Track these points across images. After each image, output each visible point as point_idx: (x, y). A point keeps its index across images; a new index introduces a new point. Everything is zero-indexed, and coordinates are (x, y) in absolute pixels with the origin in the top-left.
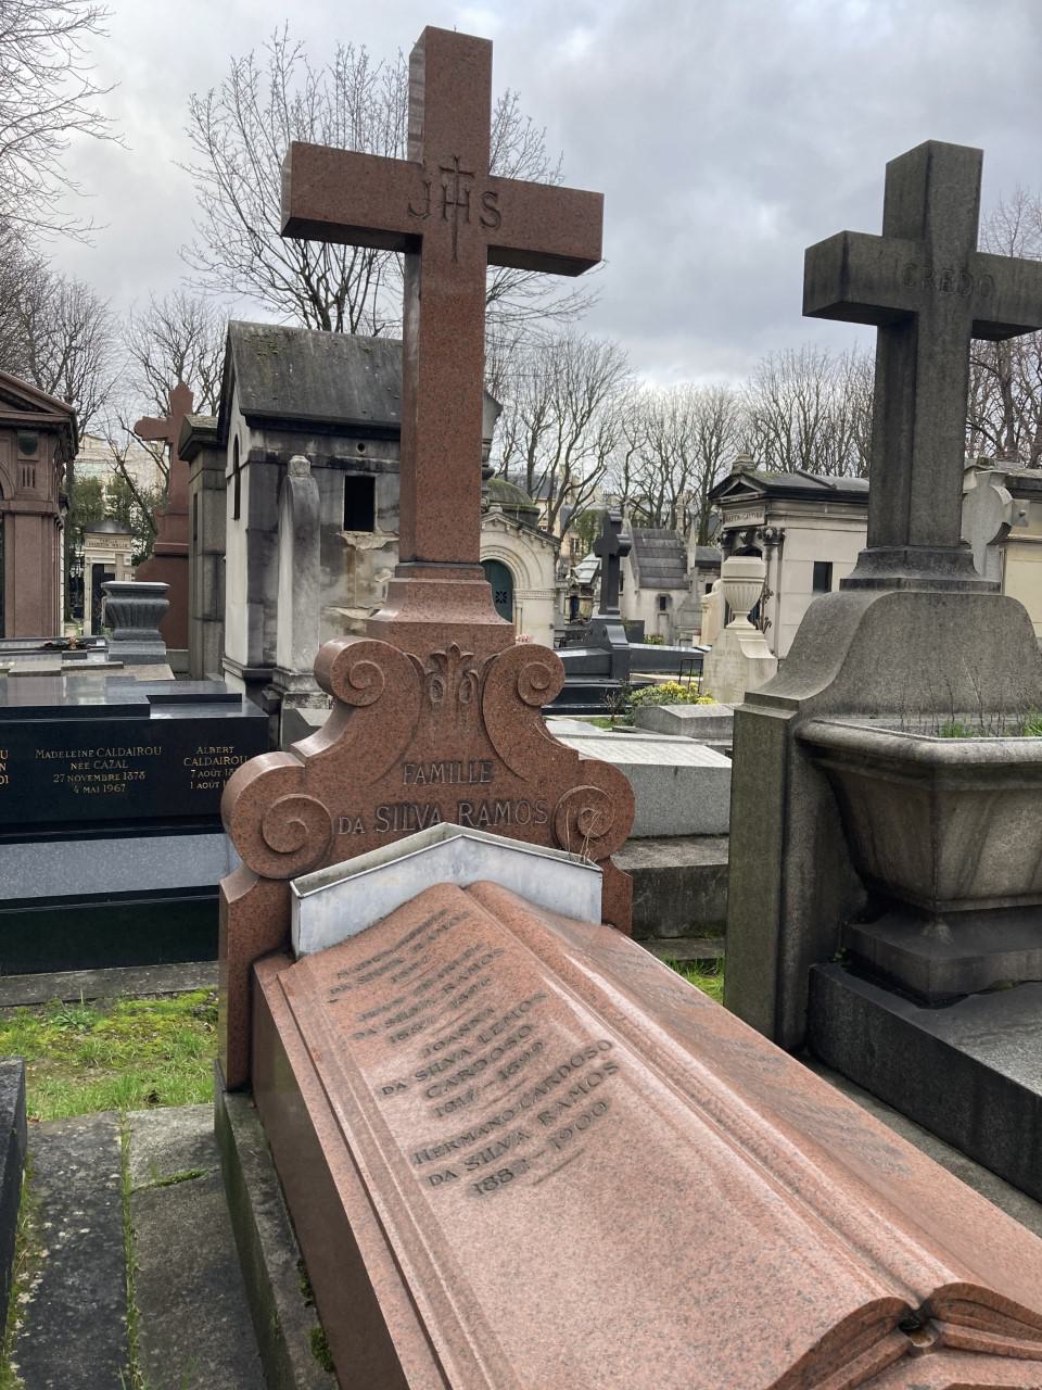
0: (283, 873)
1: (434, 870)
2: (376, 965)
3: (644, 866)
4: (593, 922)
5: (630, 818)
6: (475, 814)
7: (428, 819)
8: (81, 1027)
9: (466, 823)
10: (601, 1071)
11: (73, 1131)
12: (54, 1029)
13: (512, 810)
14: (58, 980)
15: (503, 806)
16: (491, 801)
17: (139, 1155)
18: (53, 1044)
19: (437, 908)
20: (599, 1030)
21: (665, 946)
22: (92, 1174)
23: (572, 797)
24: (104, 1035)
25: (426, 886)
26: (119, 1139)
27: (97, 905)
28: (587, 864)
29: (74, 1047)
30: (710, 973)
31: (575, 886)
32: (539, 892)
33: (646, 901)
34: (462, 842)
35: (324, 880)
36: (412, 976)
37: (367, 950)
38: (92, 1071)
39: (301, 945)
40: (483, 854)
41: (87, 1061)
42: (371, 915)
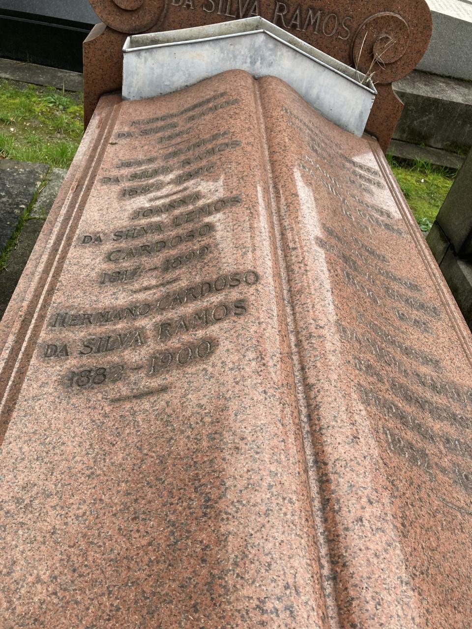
0: (125, 28)
1: (235, 57)
2: (160, 124)
3: (437, 96)
4: (356, 133)
5: (420, 53)
6: (289, 16)
7: (248, 10)
8: (61, 107)
9: (279, 23)
10: (232, 306)
11: (17, 170)
12: (46, 104)
13: (321, 20)
14: (60, 74)
15: (315, 13)
16: (305, 7)
17: (45, 197)
18: (42, 113)
19: (221, 89)
20: (264, 261)
21: (429, 152)
22: (10, 201)
23: (376, 21)
24: (72, 116)
25: (226, 69)
26: (39, 183)
27: (38, 22)
28: (368, 85)
29: (54, 118)
30: (450, 177)
31: (352, 102)
32: (318, 98)
33: (428, 121)
34: (262, 38)
35: (154, 41)
36: (173, 142)
37: (162, 109)
38: (59, 135)
39: (125, 92)
40: (279, 53)
41: (58, 129)
42: (179, 80)
